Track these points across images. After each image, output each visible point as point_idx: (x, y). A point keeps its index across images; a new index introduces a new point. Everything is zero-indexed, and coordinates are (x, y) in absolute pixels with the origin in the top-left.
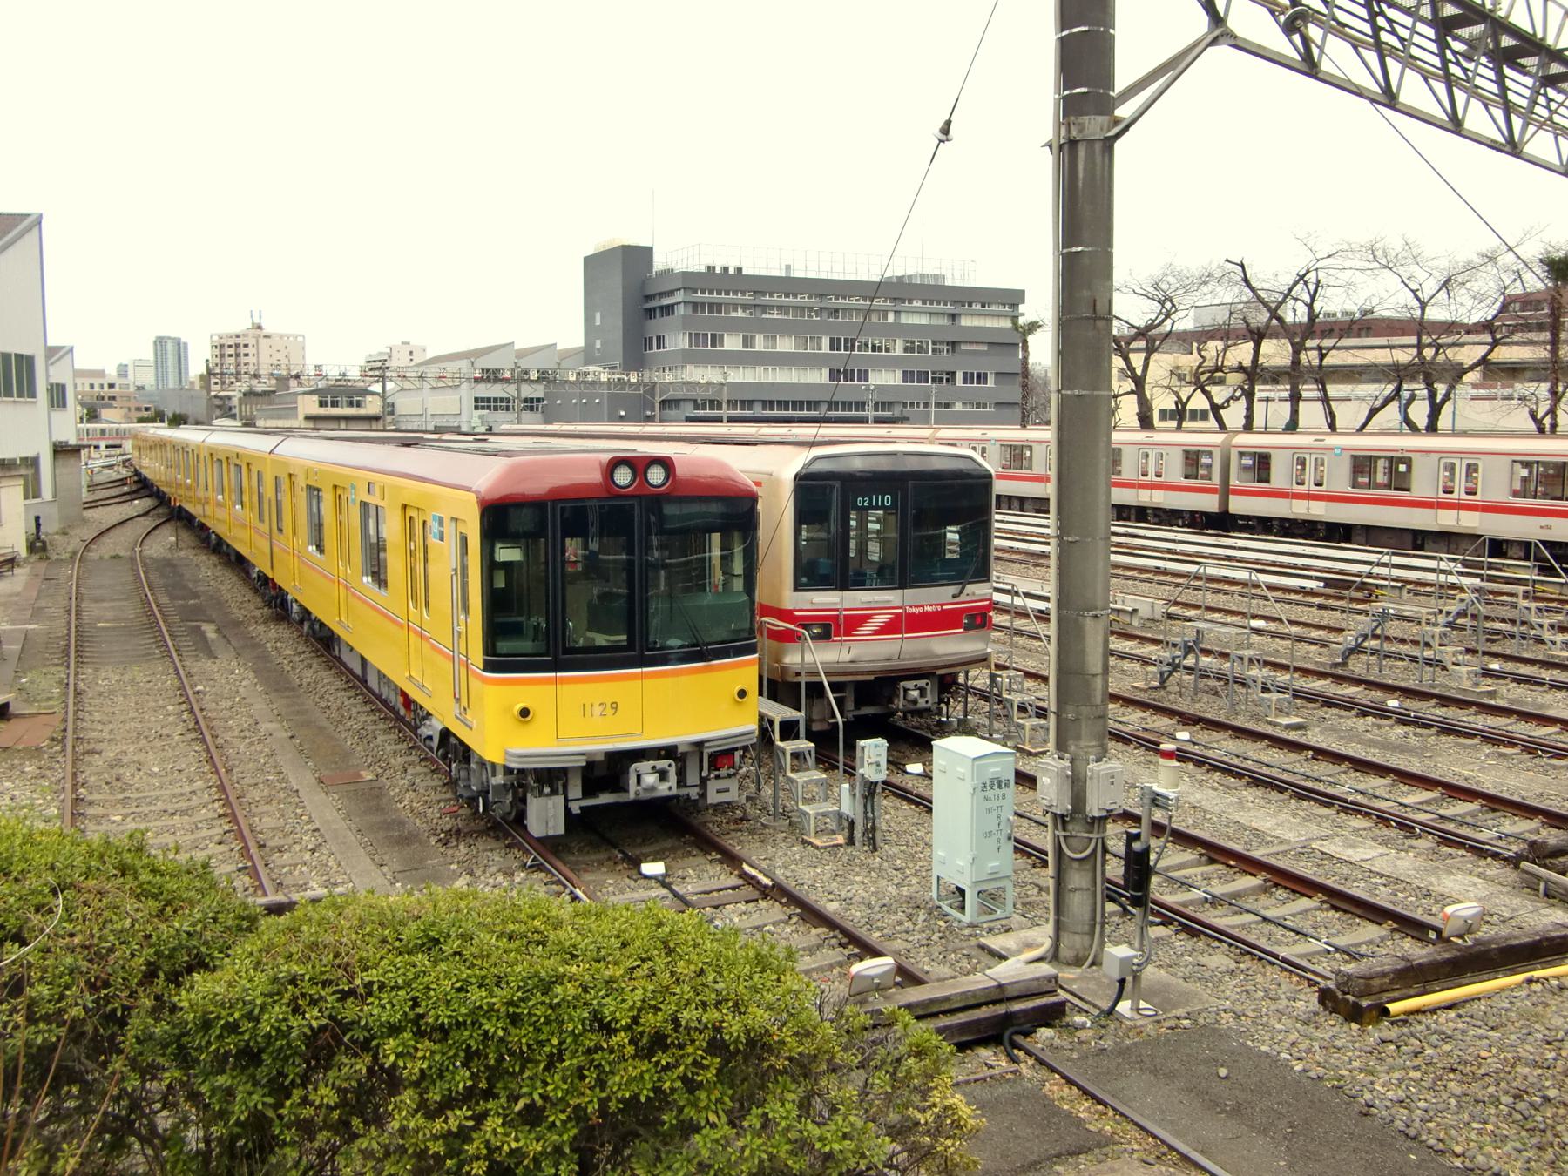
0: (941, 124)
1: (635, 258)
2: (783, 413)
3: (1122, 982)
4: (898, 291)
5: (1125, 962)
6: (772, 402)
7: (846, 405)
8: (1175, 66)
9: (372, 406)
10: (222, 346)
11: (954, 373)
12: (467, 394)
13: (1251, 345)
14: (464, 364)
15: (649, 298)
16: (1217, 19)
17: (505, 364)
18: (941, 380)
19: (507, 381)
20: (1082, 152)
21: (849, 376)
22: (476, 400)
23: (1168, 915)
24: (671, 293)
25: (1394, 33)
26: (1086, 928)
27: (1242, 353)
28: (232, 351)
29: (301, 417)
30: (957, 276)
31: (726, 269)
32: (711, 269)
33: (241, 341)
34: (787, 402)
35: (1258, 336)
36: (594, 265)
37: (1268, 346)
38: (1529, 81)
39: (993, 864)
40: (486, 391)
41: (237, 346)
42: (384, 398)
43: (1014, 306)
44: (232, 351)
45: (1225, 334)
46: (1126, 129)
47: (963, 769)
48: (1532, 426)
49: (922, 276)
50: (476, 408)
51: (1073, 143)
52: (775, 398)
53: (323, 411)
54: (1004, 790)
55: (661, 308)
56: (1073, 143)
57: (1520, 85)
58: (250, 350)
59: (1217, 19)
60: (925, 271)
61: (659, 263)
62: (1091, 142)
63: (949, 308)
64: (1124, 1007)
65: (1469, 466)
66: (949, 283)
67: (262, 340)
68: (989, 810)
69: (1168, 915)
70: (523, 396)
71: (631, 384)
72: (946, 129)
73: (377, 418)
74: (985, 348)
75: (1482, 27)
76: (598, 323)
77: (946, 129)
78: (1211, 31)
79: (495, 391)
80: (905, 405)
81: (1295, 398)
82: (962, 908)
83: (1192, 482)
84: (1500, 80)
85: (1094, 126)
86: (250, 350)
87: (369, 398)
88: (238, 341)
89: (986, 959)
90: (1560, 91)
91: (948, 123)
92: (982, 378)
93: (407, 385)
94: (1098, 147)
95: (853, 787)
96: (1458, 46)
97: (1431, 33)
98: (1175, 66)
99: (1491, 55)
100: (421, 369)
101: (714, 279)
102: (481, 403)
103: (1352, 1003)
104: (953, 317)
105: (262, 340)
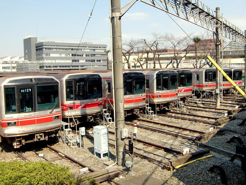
1: (194, 39)
18: (93, 61)
19: (9, 63)
21: (75, 61)
35: (148, 52)
46: (123, 15)
50: (3, 69)
55: (39, 49)
63: (94, 48)
81: (154, 63)
92: (100, 61)
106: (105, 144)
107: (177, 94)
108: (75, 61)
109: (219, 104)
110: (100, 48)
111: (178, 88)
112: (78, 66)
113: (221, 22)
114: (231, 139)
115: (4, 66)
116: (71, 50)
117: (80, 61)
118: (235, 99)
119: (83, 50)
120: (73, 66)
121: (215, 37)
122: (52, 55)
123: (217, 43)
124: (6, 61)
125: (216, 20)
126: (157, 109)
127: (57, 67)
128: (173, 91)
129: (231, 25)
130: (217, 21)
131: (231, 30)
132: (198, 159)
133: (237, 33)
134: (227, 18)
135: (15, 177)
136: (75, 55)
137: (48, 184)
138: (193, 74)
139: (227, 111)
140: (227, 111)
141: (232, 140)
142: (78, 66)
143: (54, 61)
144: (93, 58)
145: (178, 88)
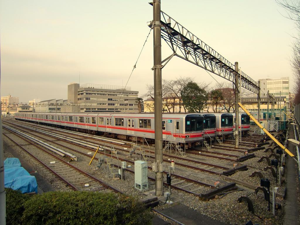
0: (134, 65)
1: (77, 86)
2: (101, 110)
3: (167, 198)
5: (168, 195)
7: (103, 109)
8: (169, 58)
9: (31, 109)
12: (47, 107)
13: (173, 100)
14: (47, 102)
16: (175, 52)
17: (54, 102)
18: (126, 105)
19: (55, 105)
20: (157, 70)
22: (49, 108)
23: (173, 187)
25: (197, 55)
26: (161, 190)
27: (172, 101)
28: (5, 100)
29: (18, 111)
31: (91, 87)
32: (89, 87)
34: (104, 109)
35: (174, 98)
36: (69, 86)
37: (176, 100)
38: (214, 63)
40: (51, 107)
42: (33, 108)
44: (5, 100)
45: (171, 98)
46: (163, 67)
47: (140, 166)
48: (213, 112)
50: (49, 110)
51: (155, 69)
52: (99, 108)
53: (22, 110)
54: (146, 169)
57: (213, 63)
59: (175, 52)
64: (168, 202)
65: (130, 126)
68: (144, 172)
69: (173, 187)
70: (58, 108)
72: (135, 66)
73: (32, 111)
75: (208, 55)
77: (135, 66)
78: (174, 53)
79: (53, 107)
81: (180, 108)
82: (140, 188)
83: (118, 126)
84: (211, 62)
85: (158, 66)
87: (30, 108)
89: (145, 196)
90: (218, 64)
91: (135, 65)
93: (37, 106)
94: (159, 69)
95: (121, 170)
96: (205, 57)
97: (202, 55)
98: (169, 58)
99: (210, 59)
100: (40, 103)
102: (50, 109)
103: (205, 197)
106: (145, 176)
107: (203, 135)
109: (237, 144)
111: (204, 129)
113: (239, 74)
114: (253, 174)
115: (50, 107)
116: (86, 94)
118: (251, 140)
119: (118, 95)
121: (234, 87)
123: (236, 91)
124: (52, 103)
125: (236, 73)
126: (186, 147)
128: (199, 133)
129: (246, 77)
130: (236, 73)
131: (247, 81)
133: (251, 84)
134: (243, 70)
136: (111, 100)
138: (84, 117)
139: (247, 150)
140: (247, 150)
141: (253, 175)
145: (204, 129)
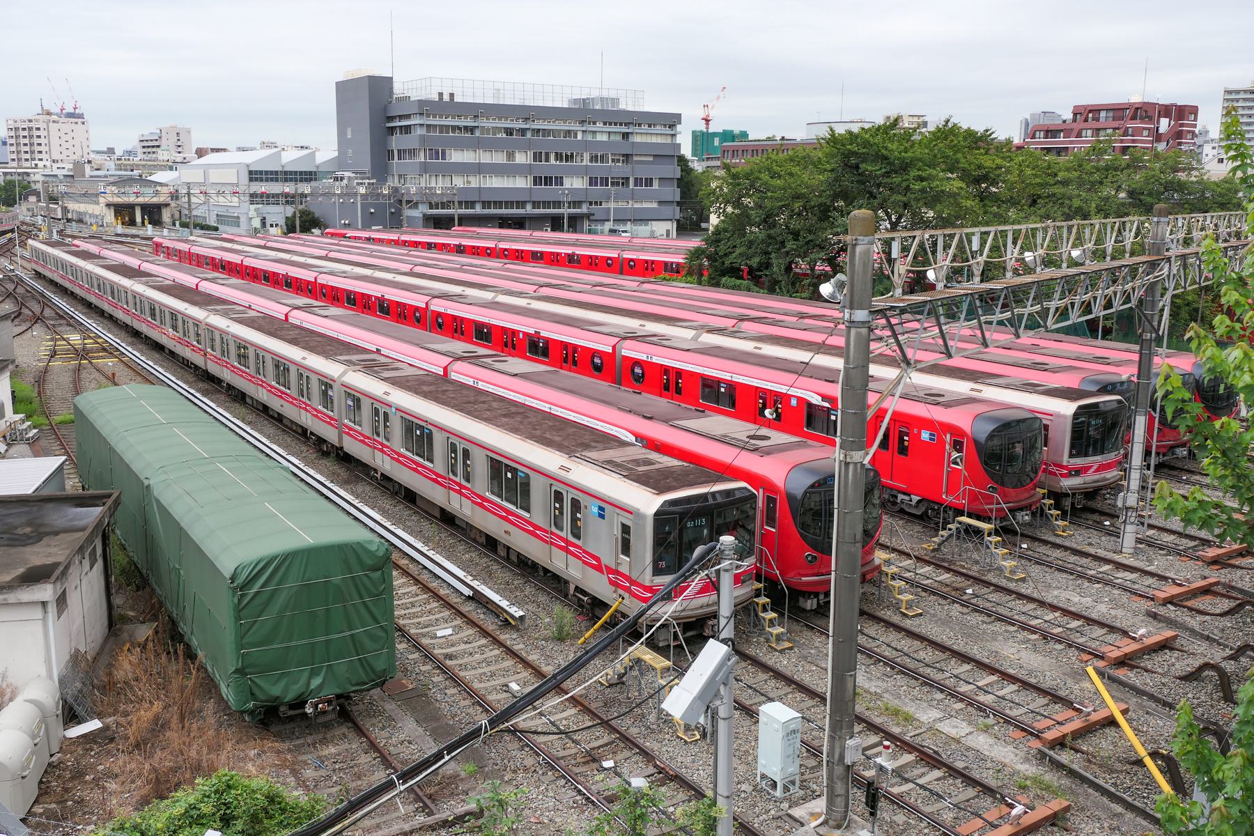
1: (379, 87)
4: (583, 113)
6: (489, 202)
10: (17, 129)
11: (628, 179)
15: (391, 119)
18: (618, 184)
20: (851, 467)
21: (548, 181)
24: (408, 117)
28: (26, 133)
30: (630, 103)
33: (33, 125)
36: (344, 88)
39: (791, 770)
41: (30, 129)
43: (672, 126)
44: (26, 133)
49: (602, 99)
55: (401, 127)
56: (847, 464)
58: (41, 141)
60: (605, 94)
61: (398, 89)
62: (856, 464)
63: (624, 129)
66: (622, 106)
67: (51, 124)
71: (385, 196)
74: (651, 159)
76: (349, 136)
80: (591, 203)
86: (41, 141)
88: (31, 125)
92: (649, 182)
101: (444, 106)
104: (626, 136)
105: (51, 124)
108: (548, 181)
110: (650, 126)
112: (558, 204)
117: (568, 183)
120: (536, 204)
122: (456, 157)
126: (1067, 503)
127: (471, 204)
132: (502, 727)
135: (172, 828)
137: (1248, 729)
142: (558, 204)
143: (459, 182)
144: (621, 169)
